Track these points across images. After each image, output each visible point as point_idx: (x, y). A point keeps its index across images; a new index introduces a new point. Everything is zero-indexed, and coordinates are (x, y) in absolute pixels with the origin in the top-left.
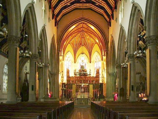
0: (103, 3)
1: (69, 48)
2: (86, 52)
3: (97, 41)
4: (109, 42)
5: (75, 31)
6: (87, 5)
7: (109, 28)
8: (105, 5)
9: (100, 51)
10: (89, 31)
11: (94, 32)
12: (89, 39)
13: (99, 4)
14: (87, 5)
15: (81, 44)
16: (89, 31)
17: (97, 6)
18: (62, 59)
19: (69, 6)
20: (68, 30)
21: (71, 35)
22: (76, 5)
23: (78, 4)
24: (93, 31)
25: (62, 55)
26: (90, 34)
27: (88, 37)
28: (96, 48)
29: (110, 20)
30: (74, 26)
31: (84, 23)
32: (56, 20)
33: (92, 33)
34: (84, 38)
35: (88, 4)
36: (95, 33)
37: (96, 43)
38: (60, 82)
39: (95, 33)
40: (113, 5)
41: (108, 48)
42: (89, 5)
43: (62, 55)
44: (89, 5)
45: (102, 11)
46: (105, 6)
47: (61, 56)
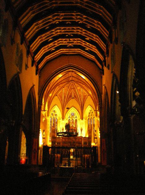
0: (93, 47)
1: (56, 100)
2: (78, 107)
3: (90, 93)
4: (102, 94)
5: (61, 81)
6: (75, 50)
7: (102, 77)
8: (96, 50)
9: (94, 105)
10: (80, 81)
11: (85, 82)
12: (81, 91)
13: (90, 39)
14: (75, 50)
15: (71, 96)
16: (80, 81)
17: (86, 51)
18: (47, 115)
19: (53, 51)
20: (55, 79)
21: (58, 85)
22: (61, 51)
23: (65, 50)
24: (84, 81)
25: (46, 108)
26: (81, 84)
27: (79, 88)
28: (89, 100)
29: (103, 67)
30: (60, 76)
31: (72, 71)
32: (37, 67)
33: (83, 83)
34: (75, 89)
35: (76, 49)
36: (87, 83)
37: (89, 95)
38: (41, 144)
39: (87, 83)
40: (105, 50)
41: (101, 100)
42: (77, 50)
43: (46, 108)
44: (77, 50)
45: (92, 57)
46: (96, 51)
47: (44, 110)
